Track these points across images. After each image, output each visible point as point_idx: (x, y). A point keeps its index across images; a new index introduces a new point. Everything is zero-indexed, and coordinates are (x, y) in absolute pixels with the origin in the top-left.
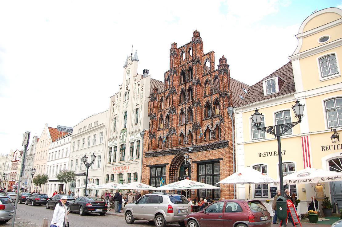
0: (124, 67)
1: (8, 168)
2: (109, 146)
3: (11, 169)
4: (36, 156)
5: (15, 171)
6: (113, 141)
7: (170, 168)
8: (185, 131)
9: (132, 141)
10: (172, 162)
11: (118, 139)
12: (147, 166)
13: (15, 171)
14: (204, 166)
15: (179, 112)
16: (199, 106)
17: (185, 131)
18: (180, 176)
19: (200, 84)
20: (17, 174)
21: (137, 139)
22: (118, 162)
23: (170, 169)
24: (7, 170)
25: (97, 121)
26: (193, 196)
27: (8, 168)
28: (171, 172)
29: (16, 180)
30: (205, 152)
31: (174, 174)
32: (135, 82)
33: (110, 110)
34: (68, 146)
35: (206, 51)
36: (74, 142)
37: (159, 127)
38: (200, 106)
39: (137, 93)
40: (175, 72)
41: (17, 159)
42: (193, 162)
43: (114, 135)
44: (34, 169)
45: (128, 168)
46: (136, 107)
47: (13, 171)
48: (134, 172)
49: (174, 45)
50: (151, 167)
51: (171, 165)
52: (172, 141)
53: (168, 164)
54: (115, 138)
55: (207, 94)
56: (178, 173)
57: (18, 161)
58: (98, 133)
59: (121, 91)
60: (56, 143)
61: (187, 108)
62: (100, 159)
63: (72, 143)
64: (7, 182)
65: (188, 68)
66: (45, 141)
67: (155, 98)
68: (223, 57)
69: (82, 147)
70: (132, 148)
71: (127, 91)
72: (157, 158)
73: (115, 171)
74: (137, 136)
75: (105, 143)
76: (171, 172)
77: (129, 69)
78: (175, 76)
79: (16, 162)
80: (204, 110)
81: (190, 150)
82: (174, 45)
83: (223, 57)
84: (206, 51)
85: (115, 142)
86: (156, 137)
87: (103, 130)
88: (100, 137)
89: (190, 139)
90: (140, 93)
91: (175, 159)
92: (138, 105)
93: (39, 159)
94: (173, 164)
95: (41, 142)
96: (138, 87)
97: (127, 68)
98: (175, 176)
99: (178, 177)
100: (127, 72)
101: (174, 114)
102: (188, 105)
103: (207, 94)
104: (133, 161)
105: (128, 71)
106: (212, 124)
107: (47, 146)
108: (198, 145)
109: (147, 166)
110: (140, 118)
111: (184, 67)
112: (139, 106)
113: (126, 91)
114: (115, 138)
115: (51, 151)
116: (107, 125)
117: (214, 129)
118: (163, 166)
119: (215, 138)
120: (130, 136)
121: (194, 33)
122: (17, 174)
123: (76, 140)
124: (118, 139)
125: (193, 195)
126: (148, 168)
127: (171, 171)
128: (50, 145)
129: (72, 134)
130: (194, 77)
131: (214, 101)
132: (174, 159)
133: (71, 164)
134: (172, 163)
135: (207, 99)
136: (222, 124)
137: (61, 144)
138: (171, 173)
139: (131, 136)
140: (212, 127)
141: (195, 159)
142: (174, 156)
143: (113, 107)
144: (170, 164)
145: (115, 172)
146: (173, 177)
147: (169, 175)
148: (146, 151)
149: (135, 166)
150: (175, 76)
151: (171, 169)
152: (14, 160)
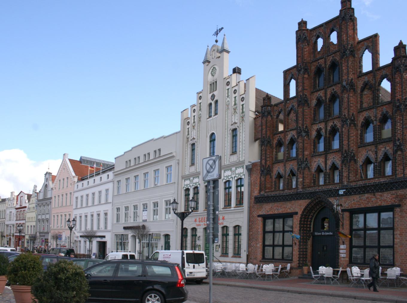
0: (204, 63)
1: (10, 218)
2: (183, 186)
3: (15, 219)
4: (53, 200)
5: (24, 222)
6: (191, 178)
7: (301, 218)
8: (326, 166)
9: (239, 177)
10: (305, 210)
11: (201, 177)
12: (259, 216)
13: (24, 222)
14: (272, 220)
15: (314, 134)
16: (352, 125)
17: (326, 166)
18: (314, 231)
19: (354, 90)
20: (26, 227)
21: (225, 178)
22: (204, 210)
23: (300, 221)
24: (10, 220)
25: (160, 150)
26: (343, 259)
27: (10, 218)
28: (302, 224)
29: (26, 233)
30: (366, 195)
31: (306, 227)
32: (228, 87)
33: (182, 133)
34: (110, 186)
35: (362, 34)
36: (119, 182)
37: (276, 158)
38: (271, 145)
39: (233, 105)
40: (306, 70)
41: (23, 206)
42: (343, 211)
43: (193, 169)
44: (71, 219)
45: (223, 219)
46: (233, 127)
47: (19, 222)
48: (234, 225)
49: (302, 24)
50: (265, 218)
51: (302, 215)
52: (303, 179)
53: (296, 213)
54: (196, 175)
55: (365, 105)
56: (312, 226)
57: (25, 207)
58: (162, 167)
59: (200, 101)
60: (85, 182)
61: (329, 128)
62: (156, 208)
63: (116, 183)
64: (12, 237)
65: (329, 63)
66: (66, 180)
67: (269, 113)
68: (401, 43)
69: (144, 187)
70: (187, 196)
71: (213, 103)
72: (276, 204)
73: (198, 223)
74: (237, 172)
75: (177, 183)
76: (302, 224)
77: (215, 66)
78: (306, 76)
79: (23, 209)
80: (359, 132)
81: (341, 192)
82: (302, 24)
83: (401, 43)
84: (362, 34)
85: (196, 180)
86: (271, 172)
87: (172, 163)
88: (126, 184)
89: (331, 176)
90: (238, 105)
91: (309, 205)
92: (194, 139)
93: (60, 206)
94: (305, 213)
95: (58, 181)
96: (234, 95)
97: (211, 65)
98: (307, 230)
99: (312, 231)
100: (211, 70)
101: (305, 138)
102: (330, 124)
103: (365, 105)
104: (232, 209)
105: (212, 68)
106: (376, 153)
107: (70, 186)
108: (353, 184)
109: (259, 216)
110: (241, 143)
111: (321, 61)
112: (238, 124)
113: (210, 101)
114: (196, 175)
115: (79, 194)
116: (179, 157)
117: (379, 160)
118: (291, 215)
119: (381, 175)
120: (183, 180)
121: (300, 24)
122: (26, 227)
123: (123, 179)
124: (201, 177)
125: (343, 258)
126: (260, 219)
127: (302, 222)
128: (76, 185)
129: (114, 168)
130: (345, 77)
131: (379, 116)
132: (308, 205)
133: (165, 207)
134: (303, 212)
135: (366, 114)
136: (399, 153)
137: (89, 186)
138: (302, 226)
139: (185, 181)
140: (376, 159)
141: (346, 206)
142: (307, 202)
143: (188, 127)
144: (300, 213)
145: (200, 225)
146: (305, 232)
147: (298, 228)
148: (256, 193)
149: (237, 216)
150: (306, 76)
151: (303, 219)
152: (18, 206)
